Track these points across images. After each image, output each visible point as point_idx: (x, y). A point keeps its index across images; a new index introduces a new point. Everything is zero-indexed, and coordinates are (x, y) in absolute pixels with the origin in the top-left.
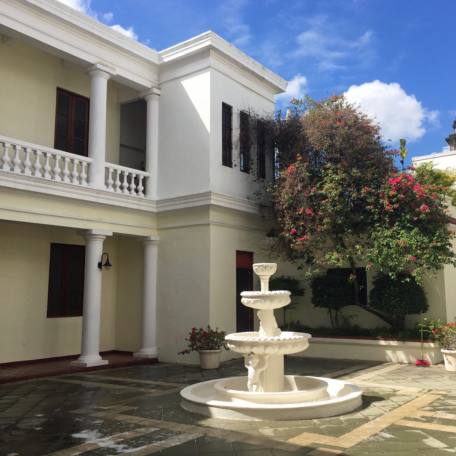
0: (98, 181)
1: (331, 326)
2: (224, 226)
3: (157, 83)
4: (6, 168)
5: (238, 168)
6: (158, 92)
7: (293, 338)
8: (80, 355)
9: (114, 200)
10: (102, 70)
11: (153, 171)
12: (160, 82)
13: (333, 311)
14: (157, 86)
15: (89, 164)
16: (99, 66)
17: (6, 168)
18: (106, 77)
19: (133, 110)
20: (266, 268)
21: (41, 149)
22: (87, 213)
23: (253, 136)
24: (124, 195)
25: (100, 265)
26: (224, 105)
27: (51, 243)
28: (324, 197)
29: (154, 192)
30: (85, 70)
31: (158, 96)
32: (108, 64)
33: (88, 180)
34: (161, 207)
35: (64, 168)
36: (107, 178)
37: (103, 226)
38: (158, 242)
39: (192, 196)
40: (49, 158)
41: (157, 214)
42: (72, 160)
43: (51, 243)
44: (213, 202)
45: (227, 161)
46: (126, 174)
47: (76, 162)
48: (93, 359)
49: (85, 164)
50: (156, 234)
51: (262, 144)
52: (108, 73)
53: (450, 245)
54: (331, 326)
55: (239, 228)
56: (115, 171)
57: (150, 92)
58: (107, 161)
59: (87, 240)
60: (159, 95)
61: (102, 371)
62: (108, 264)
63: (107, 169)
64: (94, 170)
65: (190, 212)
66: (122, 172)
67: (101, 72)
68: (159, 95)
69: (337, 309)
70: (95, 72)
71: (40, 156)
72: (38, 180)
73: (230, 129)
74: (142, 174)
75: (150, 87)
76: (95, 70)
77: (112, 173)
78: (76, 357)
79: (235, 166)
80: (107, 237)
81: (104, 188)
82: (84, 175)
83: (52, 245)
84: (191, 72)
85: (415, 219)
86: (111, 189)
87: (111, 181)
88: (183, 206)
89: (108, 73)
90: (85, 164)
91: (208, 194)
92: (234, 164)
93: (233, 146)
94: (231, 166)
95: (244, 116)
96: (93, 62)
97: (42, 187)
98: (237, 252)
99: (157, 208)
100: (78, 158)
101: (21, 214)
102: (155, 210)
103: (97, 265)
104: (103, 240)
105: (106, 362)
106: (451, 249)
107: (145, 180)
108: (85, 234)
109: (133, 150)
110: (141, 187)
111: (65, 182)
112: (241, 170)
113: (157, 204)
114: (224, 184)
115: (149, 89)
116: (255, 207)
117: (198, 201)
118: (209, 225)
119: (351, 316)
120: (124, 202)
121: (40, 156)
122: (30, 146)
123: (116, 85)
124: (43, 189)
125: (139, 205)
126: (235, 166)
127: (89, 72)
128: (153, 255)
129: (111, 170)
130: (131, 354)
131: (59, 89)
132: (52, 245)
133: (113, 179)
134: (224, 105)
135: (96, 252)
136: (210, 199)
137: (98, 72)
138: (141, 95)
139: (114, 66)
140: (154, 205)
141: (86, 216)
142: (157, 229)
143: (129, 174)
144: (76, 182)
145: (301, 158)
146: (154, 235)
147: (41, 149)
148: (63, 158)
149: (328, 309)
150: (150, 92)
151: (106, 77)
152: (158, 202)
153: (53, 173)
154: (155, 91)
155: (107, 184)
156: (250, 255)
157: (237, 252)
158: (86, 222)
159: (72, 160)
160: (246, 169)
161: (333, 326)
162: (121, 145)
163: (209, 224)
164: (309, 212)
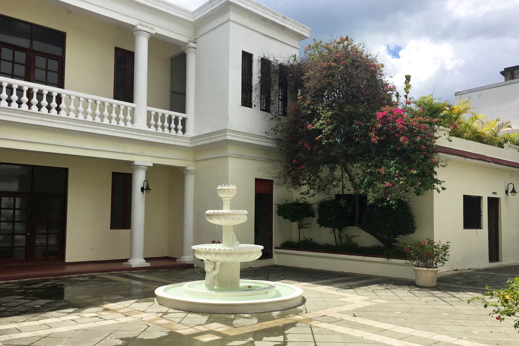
0: (141, 123)
1: (334, 244)
2: (242, 158)
5: (258, 108)
7: (222, 249)
8: (128, 259)
9: (152, 137)
11: (190, 114)
12: (196, 37)
13: (337, 231)
15: (133, 109)
16: (139, 27)
17: (4, 104)
18: (146, 36)
19: (174, 62)
20: (224, 191)
22: (130, 149)
23: (275, 79)
25: (142, 189)
26: (244, 54)
28: (319, 132)
29: (191, 132)
30: (128, 32)
32: (148, 25)
33: (132, 122)
34: (195, 142)
36: (149, 119)
37: (144, 159)
39: (214, 133)
40: (99, 105)
41: (193, 148)
42: (119, 106)
44: (229, 138)
45: (246, 102)
46: (174, 117)
47: (122, 107)
48: (138, 261)
49: (129, 109)
50: (193, 165)
51: (283, 85)
53: (435, 173)
54: (334, 244)
55: (261, 161)
56: (157, 114)
57: (187, 46)
58: (148, 105)
59: (132, 170)
60: (195, 48)
62: (148, 188)
63: (149, 113)
64: (137, 114)
65: (214, 147)
68: (195, 48)
69: (340, 230)
71: (91, 103)
73: (251, 74)
74: (181, 116)
75: (187, 42)
76: (136, 31)
77: (108, 107)
78: (126, 260)
79: (255, 106)
80: (149, 167)
81: (146, 128)
82: (129, 117)
83: (114, 174)
84: (214, 27)
85: (398, 149)
86: (153, 129)
87: (153, 122)
88: (208, 142)
90: (129, 109)
91: (224, 131)
92: (253, 105)
93: (253, 89)
94: (250, 107)
95: (265, 62)
96: (135, 25)
98: (256, 180)
99: (192, 143)
100: (123, 104)
102: (190, 145)
103: (140, 189)
105: (148, 264)
106: (435, 177)
107: (184, 121)
108: (130, 164)
109: (176, 97)
110: (180, 127)
111: (79, 118)
112: (261, 110)
113: (191, 140)
114: (246, 122)
115: (186, 44)
116: (272, 141)
117: (218, 137)
118: (227, 157)
119: (354, 236)
121: (91, 103)
123: (156, 42)
125: (175, 141)
126: (255, 106)
128: (190, 183)
129: (153, 113)
130: (175, 259)
131: (117, 49)
132: (114, 174)
134: (244, 54)
135: (139, 179)
136: (226, 135)
137: (139, 32)
138: (182, 50)
139: (152, 26)
141: (129, 151)
142: (194, 161)
144: (122, 124)
145: (301, 97)
146: (190, 166)
148: (126, 108)
149: (332, 229)
150: (187, 46)
152: (192, 138)
154: (192, 45)
155: (149, 125)
156: (270, 183)
157: (256, 180)
159: (119, 106)
160: (266, 108)
161: (337, 243)
162: (172, 92)
163: (227, 157)
164: (306, 145)
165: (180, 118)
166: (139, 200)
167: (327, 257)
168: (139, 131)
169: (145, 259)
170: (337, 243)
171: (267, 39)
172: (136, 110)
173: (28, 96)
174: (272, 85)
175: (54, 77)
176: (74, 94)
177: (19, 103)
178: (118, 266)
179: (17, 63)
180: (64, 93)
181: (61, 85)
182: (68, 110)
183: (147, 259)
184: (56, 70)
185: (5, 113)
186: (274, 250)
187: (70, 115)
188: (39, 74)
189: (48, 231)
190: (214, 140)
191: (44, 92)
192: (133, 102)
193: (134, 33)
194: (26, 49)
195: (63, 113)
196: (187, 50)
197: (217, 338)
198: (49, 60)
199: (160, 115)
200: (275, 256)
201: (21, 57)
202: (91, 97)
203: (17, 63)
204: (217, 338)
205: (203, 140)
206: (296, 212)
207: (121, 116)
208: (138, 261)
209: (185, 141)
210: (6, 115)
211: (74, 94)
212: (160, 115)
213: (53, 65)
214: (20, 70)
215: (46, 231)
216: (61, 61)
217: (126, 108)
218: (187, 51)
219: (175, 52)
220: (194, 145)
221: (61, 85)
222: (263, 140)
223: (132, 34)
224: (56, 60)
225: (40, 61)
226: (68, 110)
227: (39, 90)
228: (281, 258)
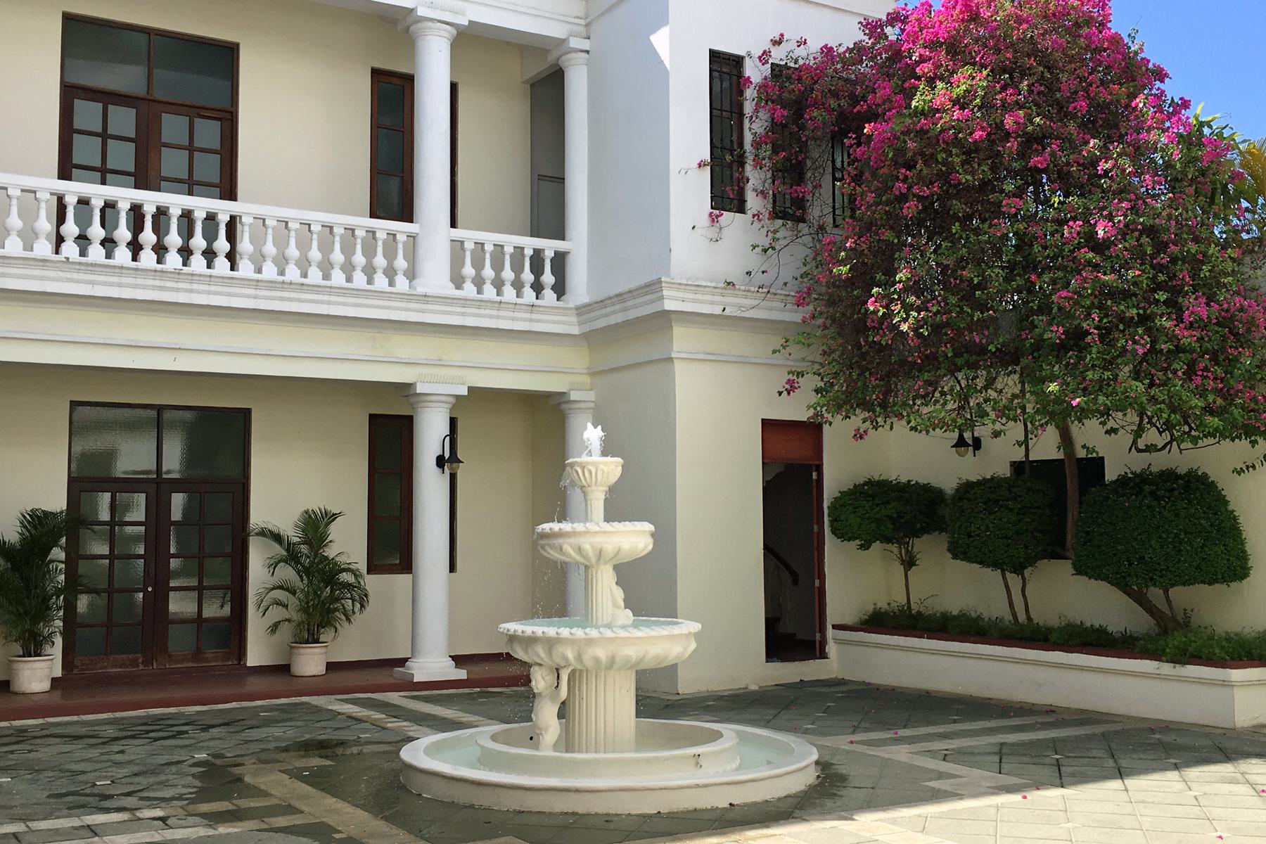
0: (435, 274)
3: (583, 22)
4: (14, 246)
6: (585, 44)
8: (406, 660)
10: (432, 20)
14: (582, 29)
15: (413, 237)
16: (421, 12)
17: (14, 246)
18: (443, 33)
21: (341, 220)
22: (405, 347)
24: (87, 264)
27: (371, 416)
31: (584, 55)
33: (411, 274)
35: (483, 267)
38: (592, 405)
43: (371, 416)
44: (669, 305)
47: (381, 235)
49: (401, 238)
52: (447, 23)
54: (1008, 617)
59: (413, 406)
60: (588, 52)
61: (466, 691)
66: (499, 247)
67: (430, 24)
68: (588, 52)
70: (419, 25)
71: (342, 236)
72: (271, 285)
74: (550, 246)
75: (563, 37)
77: (384, 242)
78: (402, 662)
80: (457, 397)
82: (401, 263)
87: (468, 270)
88: (619, 318)
89: (447, 23)
97: (290, 300)
99: (580, 324)
101: (272, 361)
102: (575, 330)
104: (449, 406)
105: (462, 674)
107: (560, 260)
108: (404, 390)
110: (222, 245)
111: (287, 278)
113: (579, 315)
114: (702, 251)
115: (563, 41)
120: (154, 288)
121: (342, 236)
122: (318, 217)
124: (212, 297)
127: (408, 27)
131: (376, 73)
133: (103, 225)
135: (431, 434)
138: (551, 58)
140: (574, 319)
143: (233, 218)
147: (341, 220)
148: (393, 236)
151: (443, 33)
152: (581, 310)
153: (83, 239)
154: (575, 43)
155: (458, 281)
156: (812, 431)
158: (403, 369)
160: (788, 209)
165: (549, 254)
166: (430, 490)
167: (980, 657)
168: (425, 298)
169: (454, 658)
170: (1015, 615)
171: (836, 15)
172: (419, 239)
173: (156, 229)
174: (790, 132)
175: (209, 167)
176: (273, 212)
177: (186, 252)
178: (381, 677)
179: (96, 134)
180: (44, 189)
181: (229, 191)
182: (258, 261)
183: (459, 660)
184: (217, 146)
185: (69, 275)
186: (830, 632)
187: (355, 277)
188: (173, 162)
189: (200, 582)
190: (632, 314)
191: (171, 211)
192: (563, 239)
193: (412, 28)
194: (137, 98)
195: (245, 268)
196: (564, 58)
197: (1168, 612)
198: (197, 121)
199: (489, 248)
200: (831, 648)
201: (124, 120)
202: (318, 217)
203: (96, 134)
204: (1168, 612)
205: (607, 315)
206: (896, 514)
207: (380, 261)
208: (432, 664)
209: (557, 318)
210: (71, 280)
211: (273, 212)
212: (489, 248)
213: (208, 133)
214: (122, 156)
215: (194, 582)
216: (228, 119)
217: (393, 236)
218: (564, 62)
219: (536, 69)
220: (587, 328)
221: (229, 191)
222: (710, 298)
223: (407, 30)
224: (215, 119)
225: (173, 127)
226: (258, 261)
227: (158, 208)
228: (841, 658)
